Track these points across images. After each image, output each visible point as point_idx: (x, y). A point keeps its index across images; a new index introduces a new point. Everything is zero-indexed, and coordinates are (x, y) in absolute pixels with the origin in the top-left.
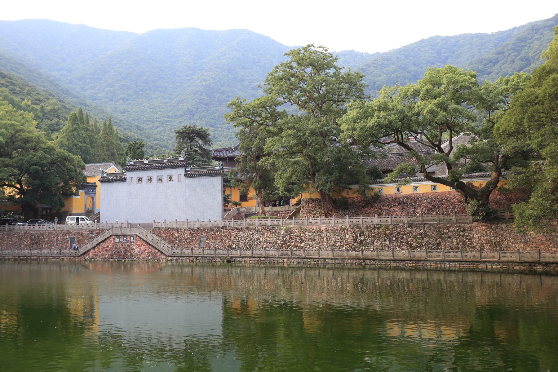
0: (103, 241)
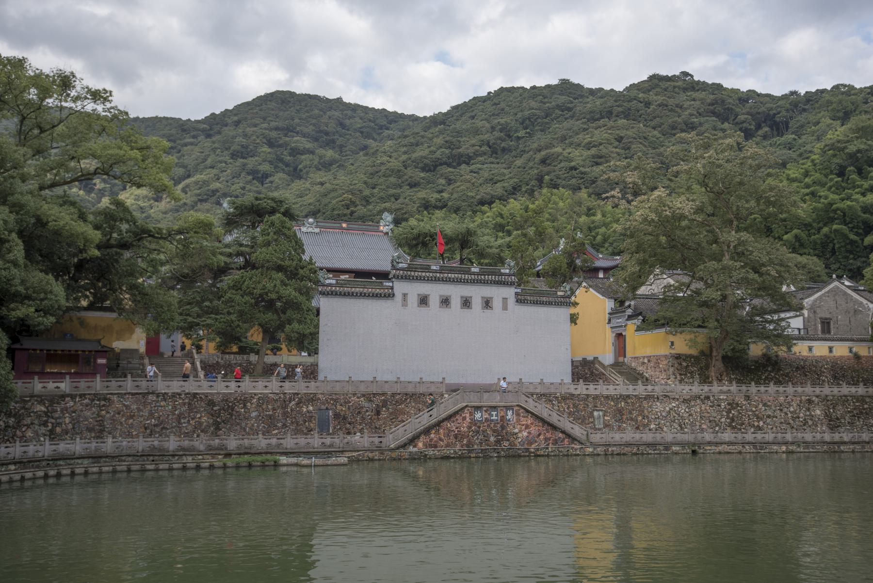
0: (449, 418)
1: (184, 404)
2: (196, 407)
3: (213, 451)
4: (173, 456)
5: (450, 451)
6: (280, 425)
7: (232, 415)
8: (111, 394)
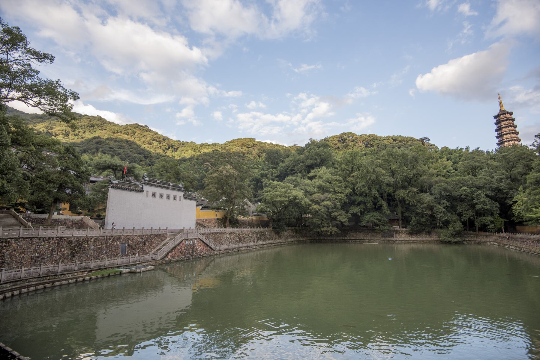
0: (178, 245)
1: (55, 243)
2: (62, 245)
3: (82, 270)
4: (61, 275)
5: (178, 259)
6: (104, 252)
7: (80, 248)
8: (10, 238)
